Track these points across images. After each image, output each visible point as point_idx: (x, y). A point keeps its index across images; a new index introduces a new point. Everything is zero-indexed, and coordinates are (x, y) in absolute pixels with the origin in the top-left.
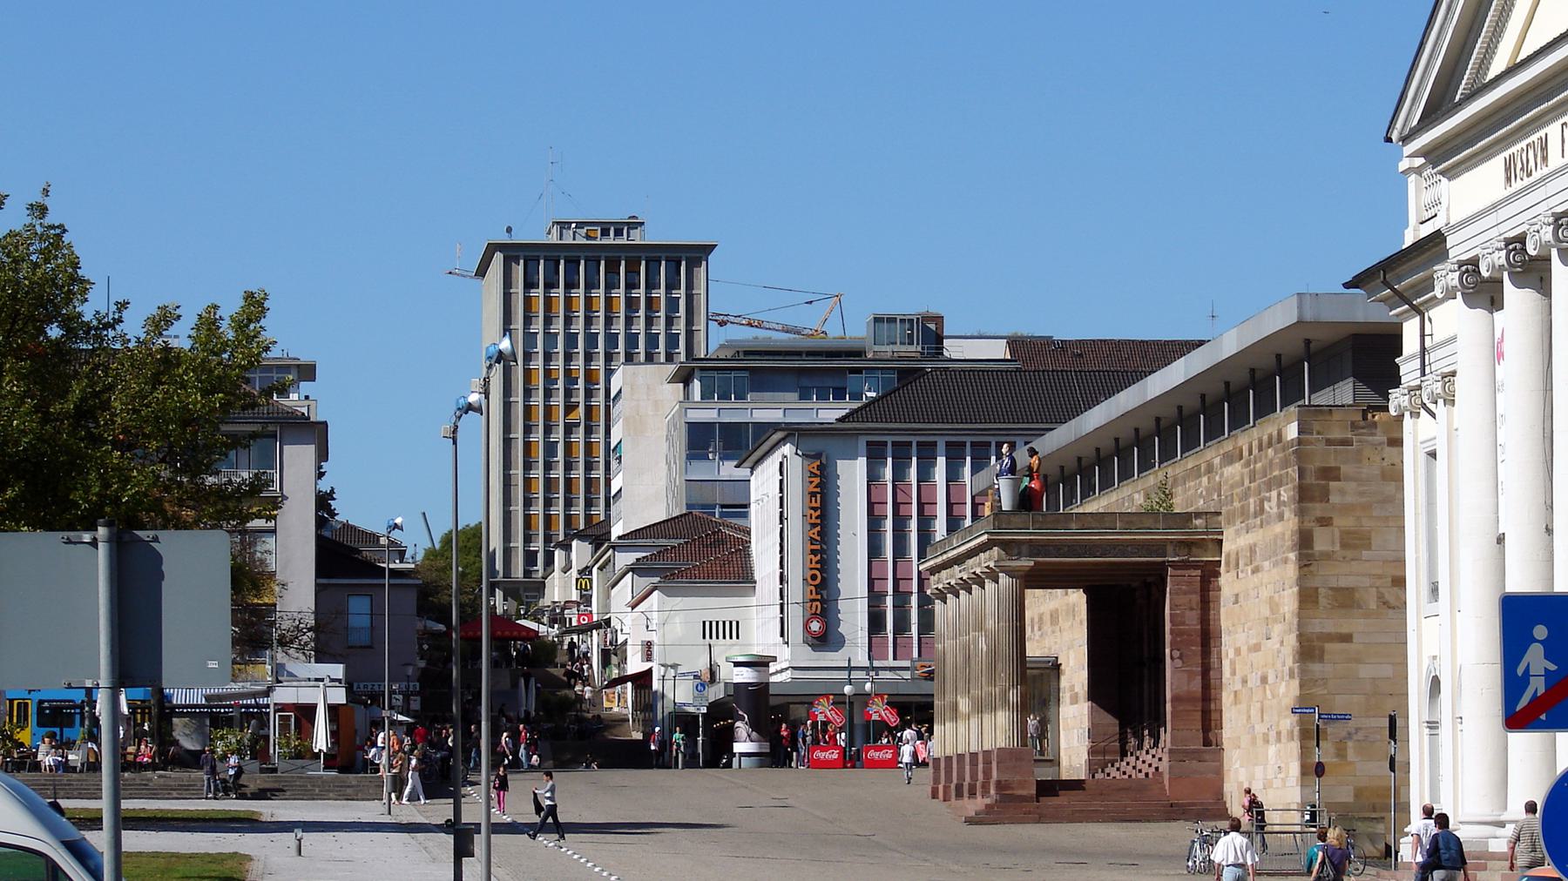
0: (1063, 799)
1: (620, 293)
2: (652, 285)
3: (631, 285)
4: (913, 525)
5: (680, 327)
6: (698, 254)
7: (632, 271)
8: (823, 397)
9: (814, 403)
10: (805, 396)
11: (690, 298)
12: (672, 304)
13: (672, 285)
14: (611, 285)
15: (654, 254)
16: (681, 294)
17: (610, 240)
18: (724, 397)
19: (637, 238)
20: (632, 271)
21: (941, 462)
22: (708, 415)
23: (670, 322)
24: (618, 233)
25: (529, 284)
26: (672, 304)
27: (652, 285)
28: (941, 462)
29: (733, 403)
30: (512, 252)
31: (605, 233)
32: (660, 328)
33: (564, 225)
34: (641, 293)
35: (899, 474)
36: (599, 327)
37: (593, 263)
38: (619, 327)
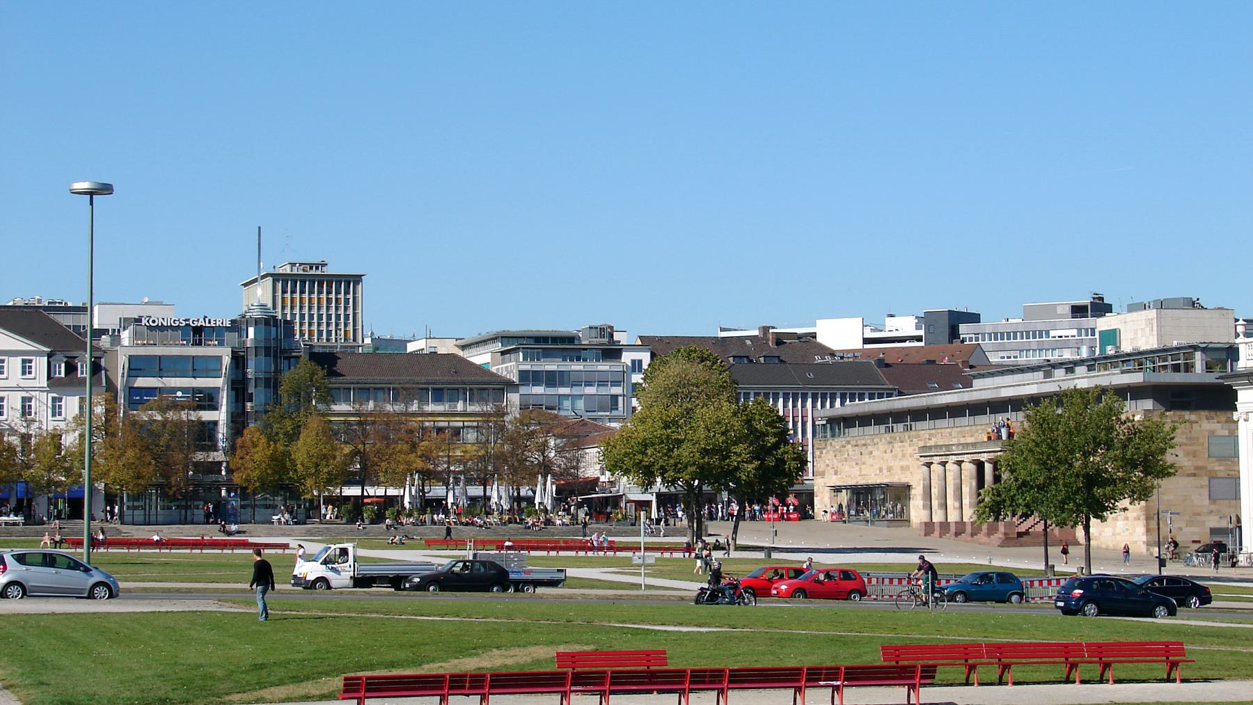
0: (1025, 538)
1: (324, 296)
2: (338, 292)
3: (329, 292)
4: (800, 424)
5: (350, 312)
6: (357, 279)
7: (329, 286)
8: (572, 360)
9: (568, 362)
10: (564, 360)
11: (354, 298)
12: (347, 301)
13: (347, 292)
14: (320, 292)
15: (339, 279)
16: (351, 296)
17: (313, 272)
18: (532, 360)
19: (328, 271)
20: (329, 286)
21: (810, 400)
22: (527, 367)
23: (346, 309)
24: (317, 268)
25: (284, 292)
26: (347, 301)
27: (338, 292)
28: (781, 400)
29: (536, 362)
30: (276, 277)
31: (311, 268)
32: (342, 312)
33: (293, 265)
34: (333, 296)
35: (794, 406)
36: (315, 311)
37: (303, 283)
38: (324, 311)
